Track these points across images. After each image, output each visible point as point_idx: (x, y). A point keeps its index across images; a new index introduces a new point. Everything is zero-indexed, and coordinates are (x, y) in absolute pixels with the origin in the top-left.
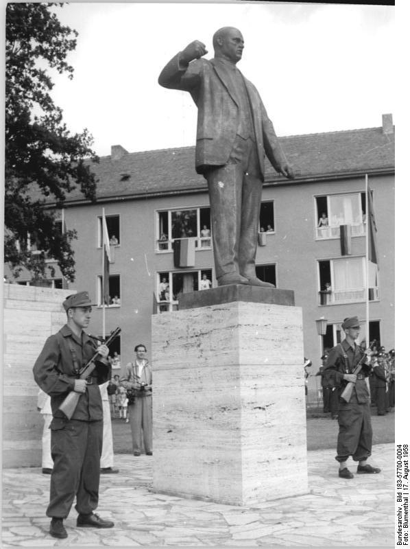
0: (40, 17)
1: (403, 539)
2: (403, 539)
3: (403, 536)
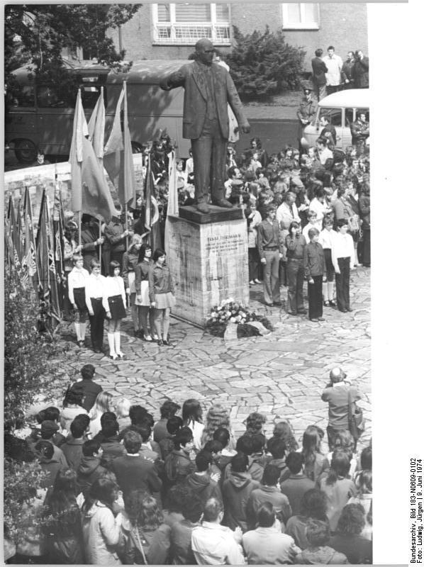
0: (259, 279)
1: (417, 557)
2: (417, 557)
3: (417, 553)
